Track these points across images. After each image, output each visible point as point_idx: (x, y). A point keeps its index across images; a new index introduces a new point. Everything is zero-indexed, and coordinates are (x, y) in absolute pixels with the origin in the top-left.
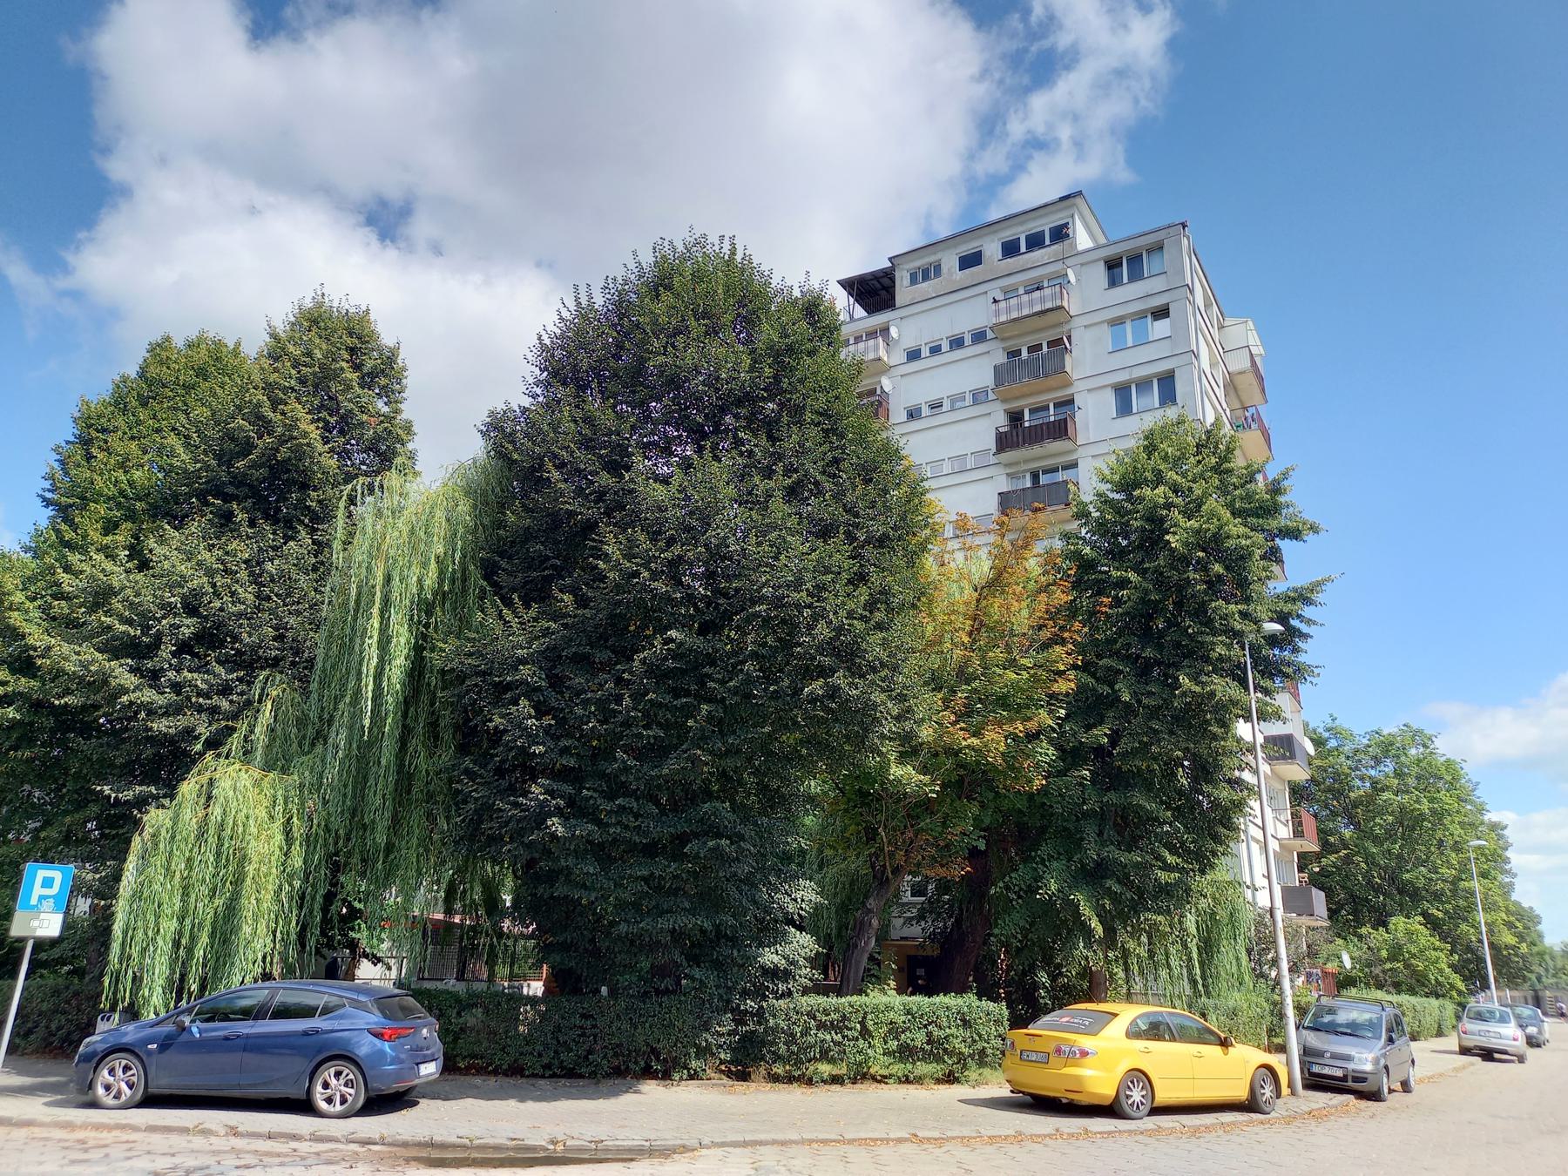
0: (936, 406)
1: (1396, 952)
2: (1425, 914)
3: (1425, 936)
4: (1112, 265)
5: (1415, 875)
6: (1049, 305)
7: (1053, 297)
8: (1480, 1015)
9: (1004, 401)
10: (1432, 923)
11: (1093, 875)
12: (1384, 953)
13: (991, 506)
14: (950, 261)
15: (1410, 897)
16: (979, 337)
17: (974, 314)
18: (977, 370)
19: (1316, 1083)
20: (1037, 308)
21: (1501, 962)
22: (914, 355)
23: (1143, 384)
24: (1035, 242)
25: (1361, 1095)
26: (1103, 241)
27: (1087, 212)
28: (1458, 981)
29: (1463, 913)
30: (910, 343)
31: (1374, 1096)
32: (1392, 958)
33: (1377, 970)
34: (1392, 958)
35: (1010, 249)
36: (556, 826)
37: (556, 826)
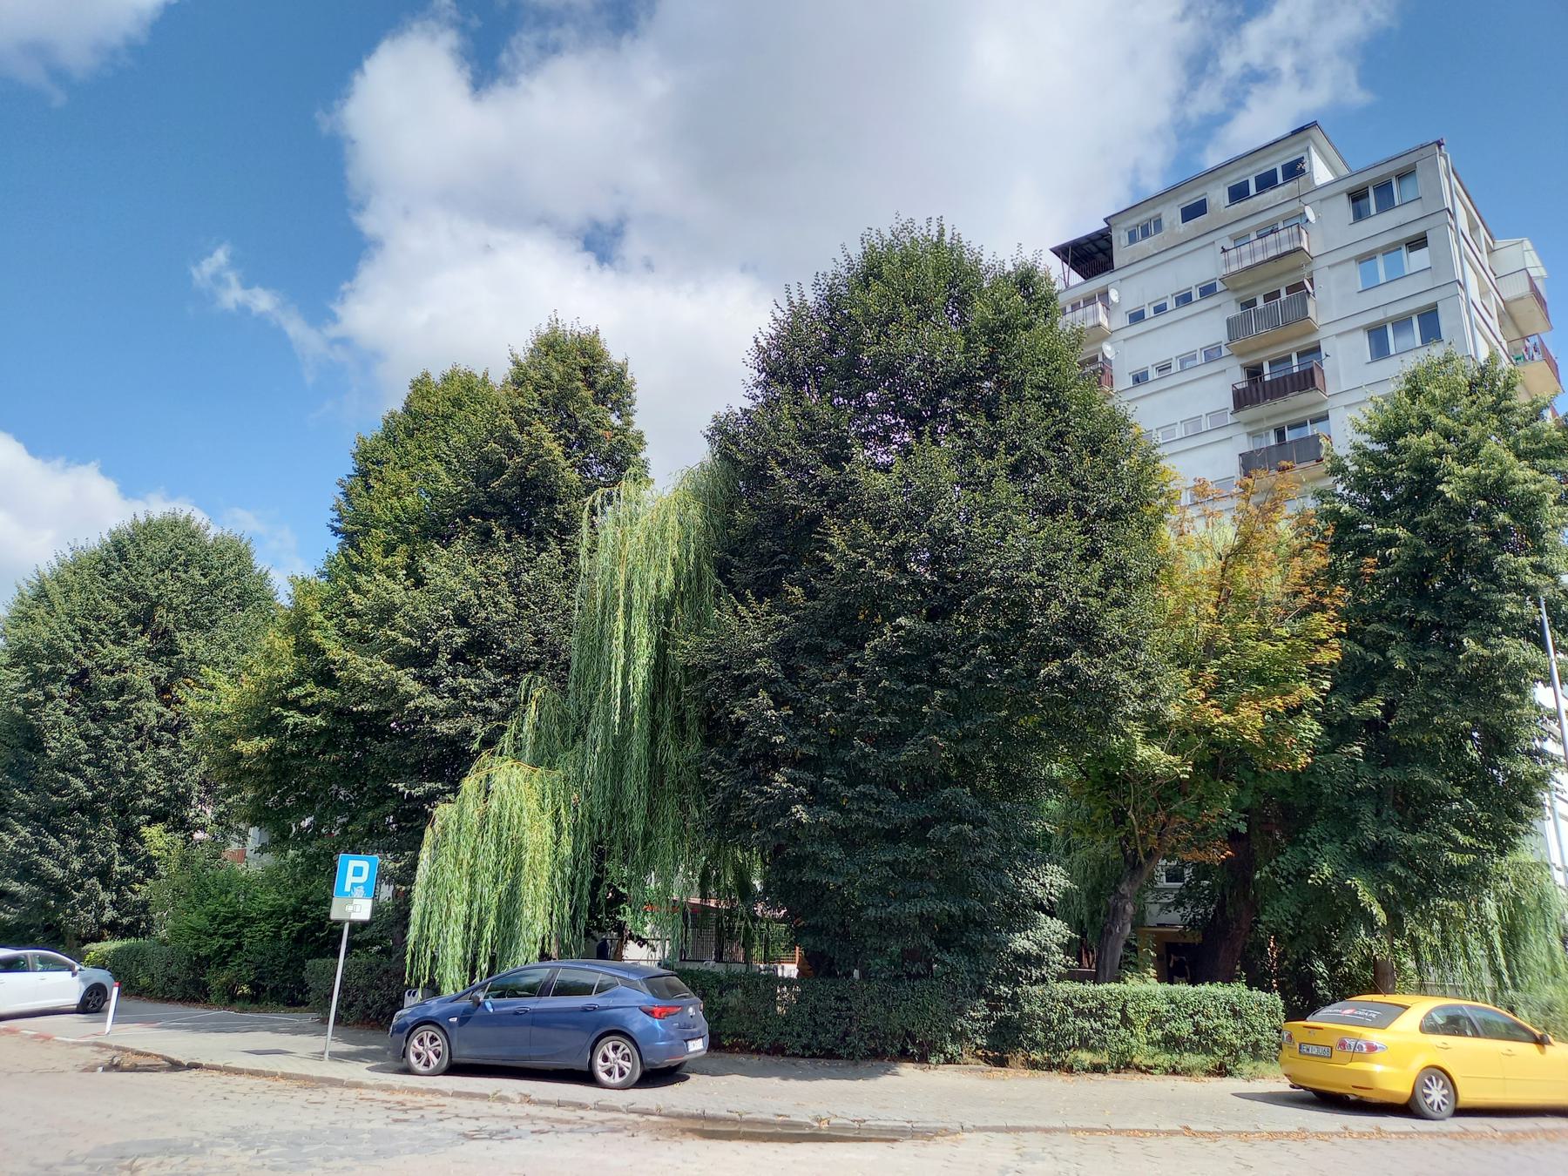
0: (1164, 368)
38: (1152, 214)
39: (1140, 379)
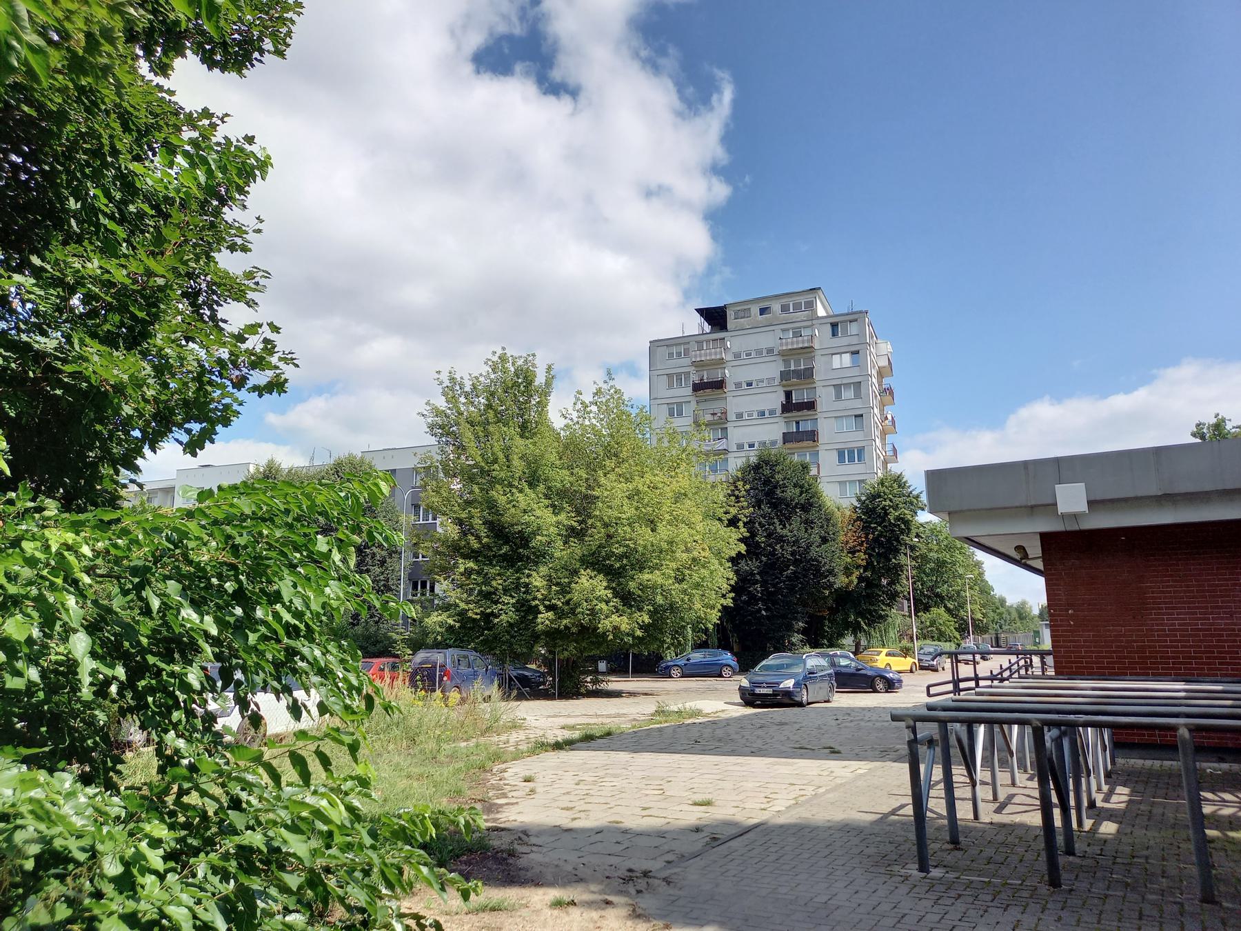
0: (749, 384)
1: (933, 623)
2: (945, 607)
3: (946, 616)
4: (834, 326)
5: (943, 589)
6: (806, 345)
7: (808, 341)
8: (715, 839)
9: (784, 386)
10: (948, 610)
11: (860, 614)
12: (928, 624)
13: (779, 437)
14: (755, 310)
15: (940, 599)
16: (770, 351)
17: (767, 340)
18: (773, 369)
19: (922, 668)
20: (801, 346)
21: (975, 626)
22: (737, 356)
23: (847, 385)
25: (933, 670)
26: (1005, 727)
27: (822, 296)
28: (957, 635)
29: (962, 606)
30: (735, 350)
31: (936, 670)
32: (931, 626)
33: (925, 631)
34: (931, 626)
35: (785, 309)
36: (764, 613)
37: (764, 613)
39: (738, 385)
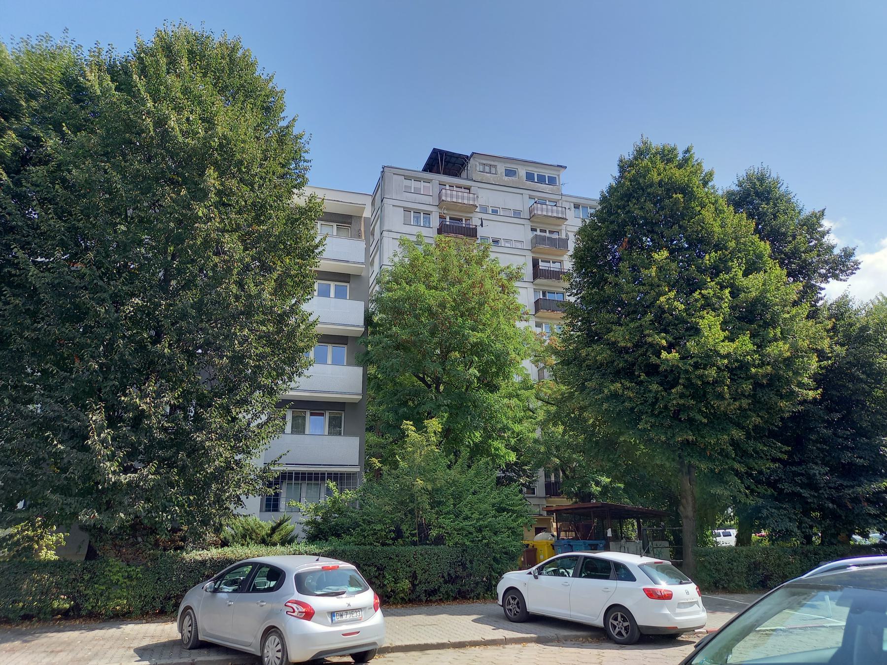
14: (501, 168)
24: (541, 179)
38: (492, 163)
